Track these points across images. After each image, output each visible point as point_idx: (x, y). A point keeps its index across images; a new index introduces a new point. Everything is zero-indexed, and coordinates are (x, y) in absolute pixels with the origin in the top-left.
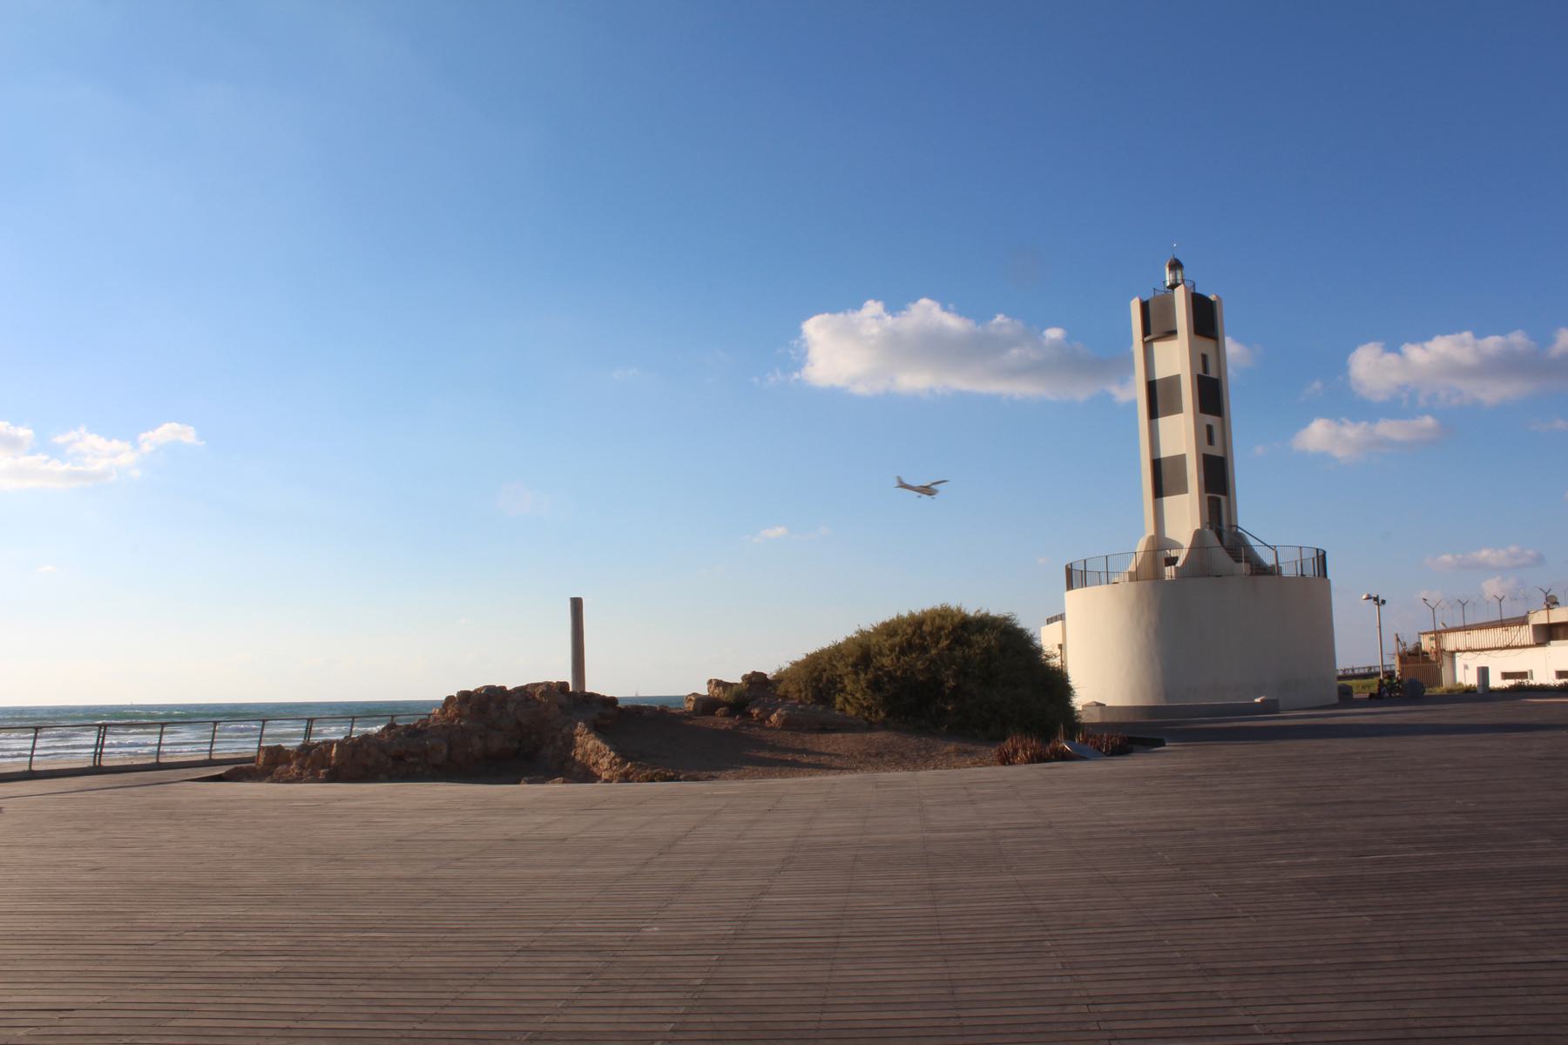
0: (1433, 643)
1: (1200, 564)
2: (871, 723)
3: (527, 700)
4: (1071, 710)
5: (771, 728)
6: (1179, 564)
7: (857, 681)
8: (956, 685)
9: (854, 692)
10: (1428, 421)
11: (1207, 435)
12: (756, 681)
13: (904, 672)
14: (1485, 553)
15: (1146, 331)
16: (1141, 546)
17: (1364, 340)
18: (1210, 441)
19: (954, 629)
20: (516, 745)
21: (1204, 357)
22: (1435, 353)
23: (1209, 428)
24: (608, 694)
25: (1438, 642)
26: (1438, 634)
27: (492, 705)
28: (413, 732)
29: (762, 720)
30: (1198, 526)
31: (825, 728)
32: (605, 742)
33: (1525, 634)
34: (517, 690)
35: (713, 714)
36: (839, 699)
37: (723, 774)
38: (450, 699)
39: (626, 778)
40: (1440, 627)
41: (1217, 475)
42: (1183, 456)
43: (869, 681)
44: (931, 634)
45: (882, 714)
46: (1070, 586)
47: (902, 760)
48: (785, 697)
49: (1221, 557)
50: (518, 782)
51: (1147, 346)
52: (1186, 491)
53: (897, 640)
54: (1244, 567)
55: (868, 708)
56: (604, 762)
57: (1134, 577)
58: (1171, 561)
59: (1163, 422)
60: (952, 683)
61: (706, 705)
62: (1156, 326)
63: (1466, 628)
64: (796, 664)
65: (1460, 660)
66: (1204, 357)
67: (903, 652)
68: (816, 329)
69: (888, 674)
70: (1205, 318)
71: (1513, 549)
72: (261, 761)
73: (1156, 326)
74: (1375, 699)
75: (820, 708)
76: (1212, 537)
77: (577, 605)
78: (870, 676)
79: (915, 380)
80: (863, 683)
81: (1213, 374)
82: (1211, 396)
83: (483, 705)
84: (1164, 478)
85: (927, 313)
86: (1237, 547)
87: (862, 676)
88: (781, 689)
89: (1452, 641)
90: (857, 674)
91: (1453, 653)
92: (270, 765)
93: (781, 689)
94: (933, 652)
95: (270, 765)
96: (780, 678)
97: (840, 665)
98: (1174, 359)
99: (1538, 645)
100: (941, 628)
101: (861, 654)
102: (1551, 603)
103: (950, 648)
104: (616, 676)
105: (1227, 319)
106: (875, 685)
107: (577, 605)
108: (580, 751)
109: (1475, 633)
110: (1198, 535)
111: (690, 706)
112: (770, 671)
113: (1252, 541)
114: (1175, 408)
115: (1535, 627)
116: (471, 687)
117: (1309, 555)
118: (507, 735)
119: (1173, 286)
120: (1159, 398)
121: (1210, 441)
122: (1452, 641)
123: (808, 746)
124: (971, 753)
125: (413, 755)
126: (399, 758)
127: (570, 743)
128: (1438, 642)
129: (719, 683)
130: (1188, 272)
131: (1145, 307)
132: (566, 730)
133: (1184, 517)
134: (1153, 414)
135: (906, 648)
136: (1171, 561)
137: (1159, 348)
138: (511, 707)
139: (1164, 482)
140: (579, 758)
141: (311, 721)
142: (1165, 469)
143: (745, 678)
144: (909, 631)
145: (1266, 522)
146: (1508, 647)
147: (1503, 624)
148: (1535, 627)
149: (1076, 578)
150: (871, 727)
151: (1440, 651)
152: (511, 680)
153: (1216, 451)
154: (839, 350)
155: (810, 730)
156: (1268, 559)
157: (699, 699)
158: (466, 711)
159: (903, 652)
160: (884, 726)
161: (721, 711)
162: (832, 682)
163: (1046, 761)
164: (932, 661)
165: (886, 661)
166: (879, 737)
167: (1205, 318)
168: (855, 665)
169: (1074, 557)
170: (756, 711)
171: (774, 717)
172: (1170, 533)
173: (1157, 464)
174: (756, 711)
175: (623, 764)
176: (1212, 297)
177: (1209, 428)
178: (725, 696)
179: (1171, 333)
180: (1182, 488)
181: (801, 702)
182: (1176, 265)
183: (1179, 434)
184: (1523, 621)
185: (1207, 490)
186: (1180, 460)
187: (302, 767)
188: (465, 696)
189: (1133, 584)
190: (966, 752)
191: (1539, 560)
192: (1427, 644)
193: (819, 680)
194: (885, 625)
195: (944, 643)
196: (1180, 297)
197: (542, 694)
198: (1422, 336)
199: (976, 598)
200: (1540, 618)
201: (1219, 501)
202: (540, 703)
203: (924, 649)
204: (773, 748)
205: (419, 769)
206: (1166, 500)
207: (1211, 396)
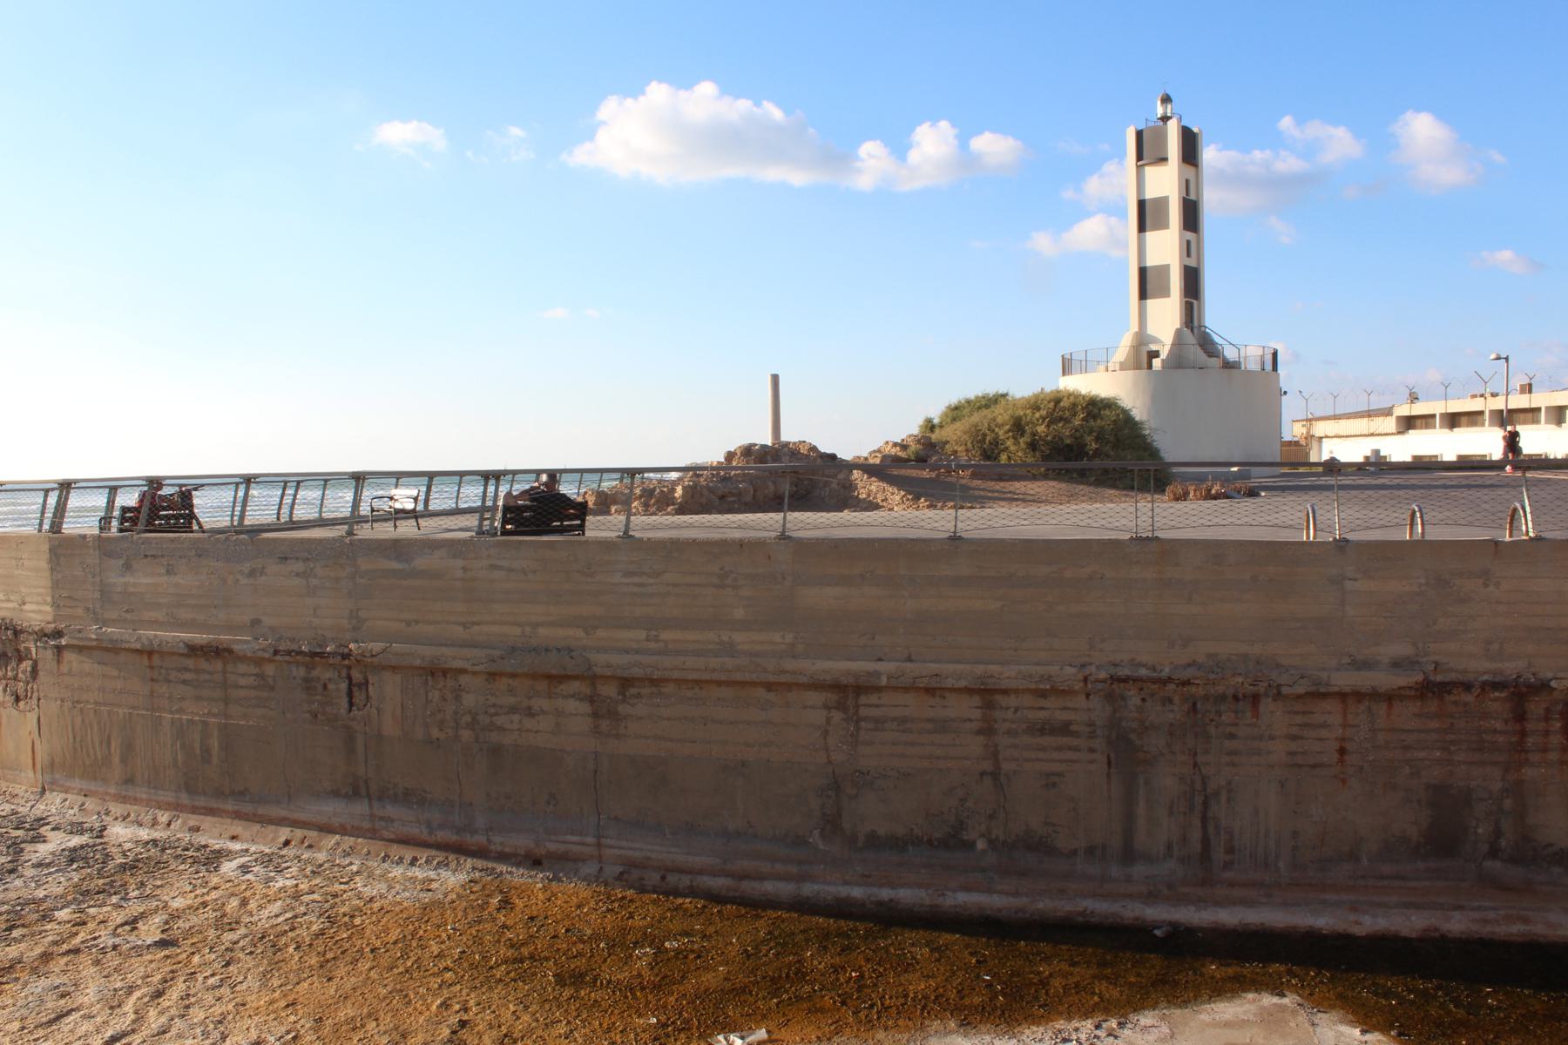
1: (1178, 361)
7: (1016, 443)
9: (1015, 451)
11: (1187, 249)
15: (1140, 157)
17: (713, 80)
18: (1189, 255)
33: (1390, 424)
38: (730, 456)
42: (1168, 266)
46: (1064, 374)
47: (1091, 500)
49: (1198, 354)
54: (1214, 361)
57: (1123, 367)
58: (1156, 354)
59: (1150, 236)
60: (1094, 446)
62: (1147, 150)
63: (1335, 417)
65: (1326, 443)
76: (1190, 338)
77: (775, 379)
80: (1023, 445)
81: (1192, 197)
82: (1191, 216)
84: (1148, 284)
86: (1207, 345)
89: (1320, 429)
98: (1164, 181)
102: (1414, 398)
105: (1209, 155)
106: (1033, 446)
107: (775, 379)
109: (1343, 422)
110: (1178, 333)
113: (1217, 339)
114: (1162, 224)
119: (1165, 119)
122: (1320, 429)
126: (722, 497)
131: (1139, 134)
133: (1165, 317)
136: (1156, 354)
145: (1236, 326)
147: (1369, 414)
149: (1075, 365)
151: (1310, 437)
153: (1192, 263)
156: (1230, 354)
165: (1041, 429)
169: (1073, 346)
176: (1195, 130)
177: (1188, 242)
179: (1164, 160)
182: (1166, 100)
183: (1165, 247)
184: (1387, 412)
186: (1164, 270)
189: (1130, 373)
200: (1404, 410)
206: (1151, 303)
207: (1191, 216)
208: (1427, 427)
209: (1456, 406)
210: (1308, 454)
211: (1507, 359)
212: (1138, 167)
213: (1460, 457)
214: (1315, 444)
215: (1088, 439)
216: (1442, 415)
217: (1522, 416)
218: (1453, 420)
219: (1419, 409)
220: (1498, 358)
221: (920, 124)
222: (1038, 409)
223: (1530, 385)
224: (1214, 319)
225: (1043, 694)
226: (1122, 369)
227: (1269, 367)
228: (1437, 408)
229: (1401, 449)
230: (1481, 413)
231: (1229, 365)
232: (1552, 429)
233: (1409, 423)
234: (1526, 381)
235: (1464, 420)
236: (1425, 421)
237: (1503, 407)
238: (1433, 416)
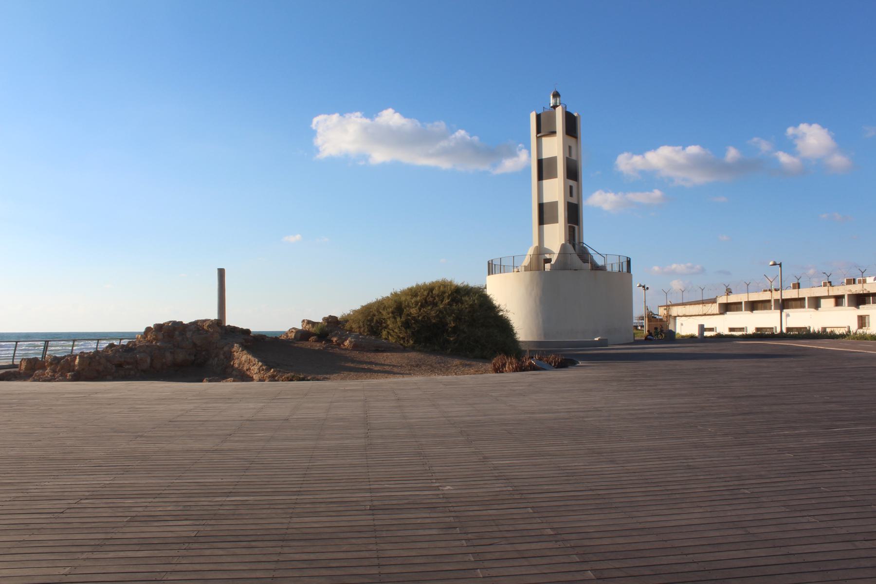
0: (665, 312)
1: (563, 264)
2: (405, 347)
3: (198, 330)
4: (516, 342)
5: (346, 349)
6: (553, 262)
7: (395, 322)
8: (446, 326)
9: (394, 329)
10: (657, 193)
12: (332, 321)
13: (424, 317)
14: (674, 266)
15: (539, 131)
16: (531, 251)
17: (622, 152)
18: (571, 195)
19: (452, 293)
20: (193, 358)
21: (570, 147)
22: (660, 157)
23: (571, 187)
24: (245, 328)
25: (668, 311)
26: (668, 307)
27: (177, 333)
28: (127, 349)
29: (339, 344)
30: (563, 242)
31: (378, 349)
32: (254, 356)
33: (715, 308)
34: (191, 324)
35: (307, 340)
36: (384, 333)
37: (332, 376)
38: (148, 329)
39: (273, 378)
40: (669, 303)
41: (574, 214)
43: (402, 323)
44: (438, 296)
45: (411, 342)
46: (490, 272)
47: (432, 369)
48: (351, 330)
50: (201, 381)
51: (539, 139)
52: (557, 222)
53: (419, 298)
55: (403, 338)
56: (255, 369)
57: (527, 269)
58: (548, 261)
59: (546, 183)
61: (303, 335)
62: (544, 128)
64: (355, 311)
66: (570, 147)
67: (422, 306)
68: (320, 122)
69: (414, 318)
70: (571, 126)
71: (689, 265)
72: (23, 367)
73: (544, 128)
74: (648, 340)
75: (373, 338)
76: (570, 247)
77: (221, 273)
78: (403, 319)
79: (380, 156)
80: (399, 324)
81: (574, 157)
83: (169, 332)
84: (545, 214)
85: (390, 118)
86: (584, 255)
87: (398, 319)
88: (347, 326)
89: (675, 311)
90: (395, 318)
91: (675, 317)
92: (32, 369)
93: (347, 326)
94: (441, 306)
95: (32, 369)
96: (345, 320)
97: (384, 313)
99: (721, 314)
100: (444, 292)
101: (397, 305)
102: (729, 292)
103: (449, 304)
104: (252, 314)
106: (406, 325)
107: (221, 273)
108: (237, 362)
109: (688, 307)
110: (563, 247)
111: (293, 335)
112: (338, 313)
113: (591, 251)
114: (553, 175)
115: (720, 304)
116: (161, 321)
117: (624, 260)
118: (189, 352)
119: (555, 107)
120: (544, 169)
121: (571, 195)
122: (675, 311)
123: (373, 360)
124: (470, 366)
125: (128, 363)
126: (120, 366)
127: (230, 356)
128: (668, 311)
129: (309, 322)
130: (563, 98)
131: (538, 117)
132: (226, 349)
133: (555, 236)
134: (540, 178)
135: (425, 303)
136: (548, 261)
137: (545, 141)
138: (189, 334)
139: (545, 216)
140: (236, 366)
141: (47, 342)
142: (545, 209)
143: (325, 319)
144: (425, 293)
146: (705, 315)
147: (703, 302)
148: (720, 304)
150: (404, 349)
151: (669, 316)
152: (187, 318)
153: (573, 200)
154: (339, 135)
155: (369, 351)
156: (600, 261)
157: (298, 331)
158: (160, 336)
159: (422, 306)
160: (413, 349)
161: (312, 338)
162: (380, 322)
163: (524, 371)
164: (441, 312)
165: (414, 311)
166: (413, 355)
167: (571, 126)
168: (393, 313)
169: (494, 256)
170: (335, 339)
171: (347, 343)
172: (547, 245)
173: (541, 206)
174: (335, 339)
175: (268, 370)
176: (575, 114)
177: (571, 187)
178: (313, 330)
179: (553, 133)
180: (555, 220)
181: (361, 334)
182: (556, 95)
183: (555, 190)
184: (713, 301)
185: (569, 222)
186: (554, 205)
187: (54, 371)
188: (159, 327)
189: (528, 273)
190: (466, 365)
191: (703, 271)
192: (662, 312)
193: (371, 321)
194: (410, 290)
195: (447, 301)
196: (559, 113)
197: (209, 326)
198: (654, 147)
199: (463, 276)
200: (723, 300)
201: (574, 228)
202: (207, 331)
203: (435, 305)
204: (353, 361)
205: (132, 372)
206: (546, 227)
208: (765, 308)
209: (754, 297)
210: (668, 326)
211: (780, 265)
212: (538, 138)
213: (758, 329)
214: (672, 321)
215: (449, 319)
216: (849, 295)
217: (793, 303)
218: (753, 306)
219: (732, 299)
220: (775, 264)
221: (386, 108)
222: (416, 295)
223: (799, 284)
224: (590, 238)
225: (280, 553)
226: (525, 270)
227: (625, 270)
228: (742, 298)
229: (723, 324)
230: (769, 301)
231: (596, 268)
232: (812, 311)
233: (727, 308)
234: (796, 282)
235: (760, 305)
236: (798, 303)
237: (779, 297)
238: (741, 303)
